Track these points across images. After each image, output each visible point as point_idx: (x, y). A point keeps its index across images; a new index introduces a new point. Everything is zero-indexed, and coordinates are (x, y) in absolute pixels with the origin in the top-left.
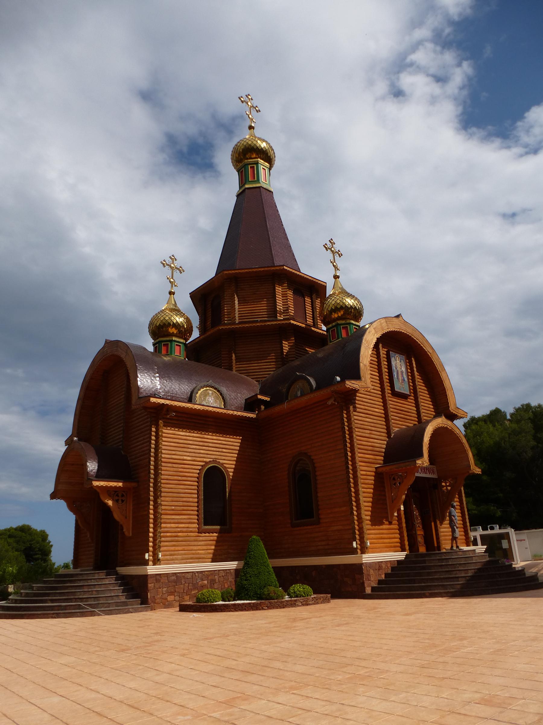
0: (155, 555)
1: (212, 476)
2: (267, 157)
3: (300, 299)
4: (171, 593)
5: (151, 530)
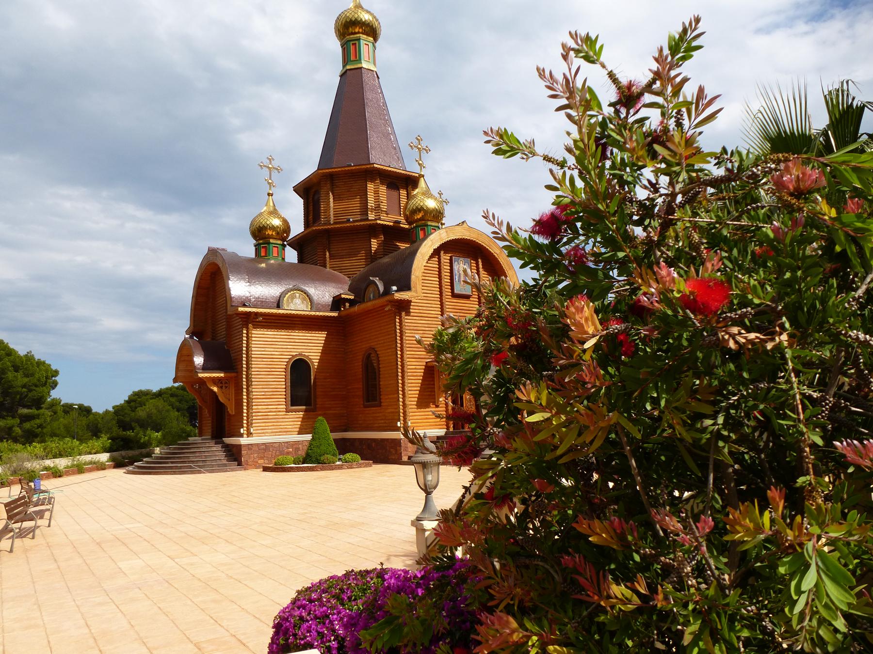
0: (248, 429)
1: (298, 368)
2: (372, 31)
3: (394, 193)
4: (262, 458)
5: (245, 411)
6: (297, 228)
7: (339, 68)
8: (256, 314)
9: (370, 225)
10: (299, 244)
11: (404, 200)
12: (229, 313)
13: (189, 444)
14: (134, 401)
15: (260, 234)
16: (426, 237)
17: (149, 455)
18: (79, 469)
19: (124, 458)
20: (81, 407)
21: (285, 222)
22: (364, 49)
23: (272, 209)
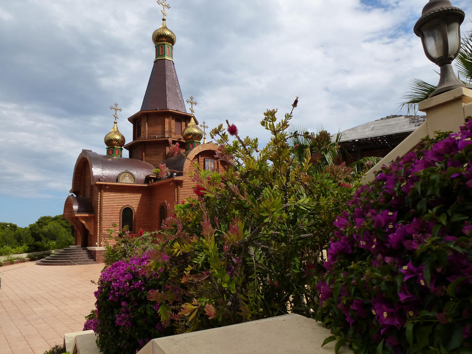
0: (100, 243)
1: (127, 212)
3: (179, 124)
6: (129, 139)
7: (154, 58)
8: (106, 185)
9: (166, 140)
10: (130, 148)
11: (184, 127)
12: (92, 184)
13: (69, 250)
14: (41, 222)
15: (109, 143)
16: (193, 147)
17: (48, 255)
18: (11, 262)
19: (35, 256)
20: (11, 225)
21: (123, 137)
22: (167, 49)
23: (116, 130)
